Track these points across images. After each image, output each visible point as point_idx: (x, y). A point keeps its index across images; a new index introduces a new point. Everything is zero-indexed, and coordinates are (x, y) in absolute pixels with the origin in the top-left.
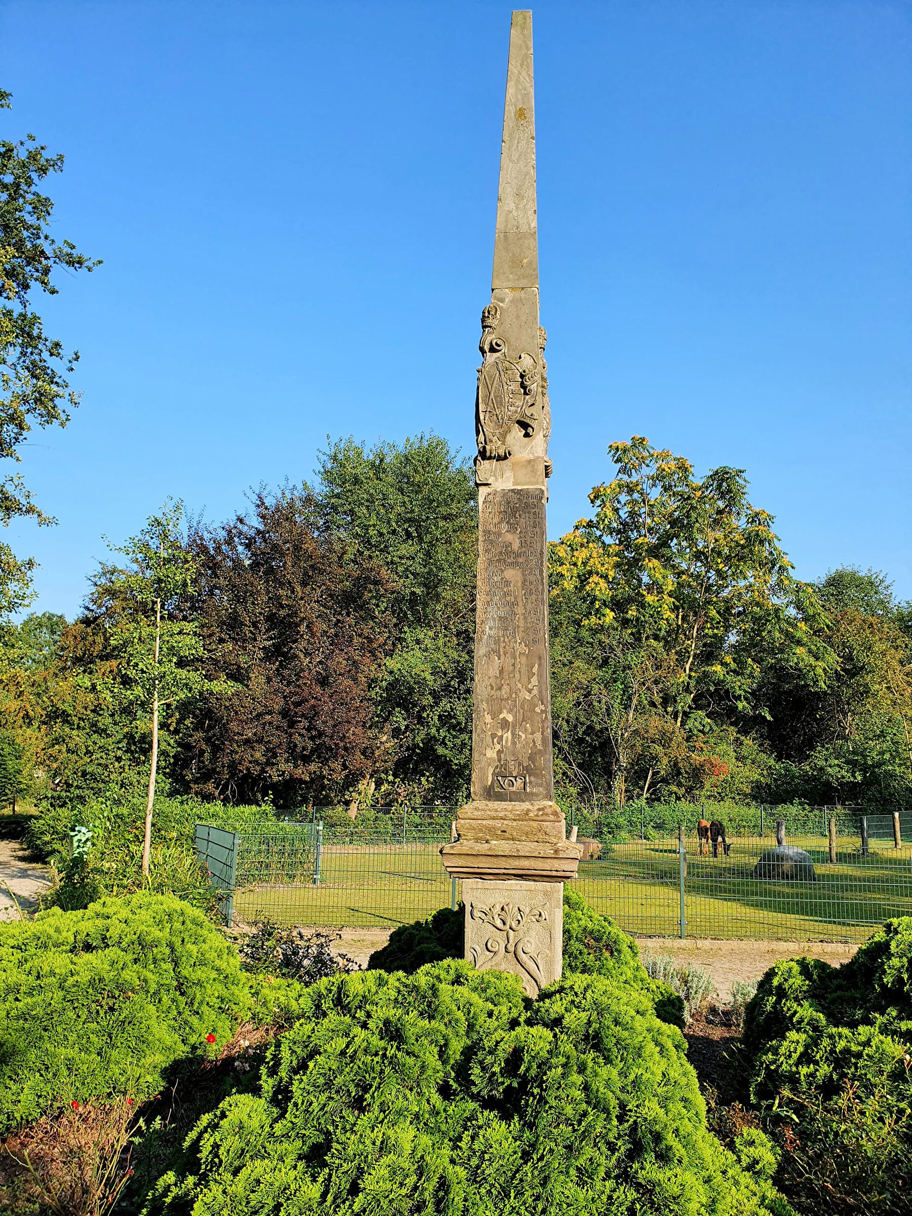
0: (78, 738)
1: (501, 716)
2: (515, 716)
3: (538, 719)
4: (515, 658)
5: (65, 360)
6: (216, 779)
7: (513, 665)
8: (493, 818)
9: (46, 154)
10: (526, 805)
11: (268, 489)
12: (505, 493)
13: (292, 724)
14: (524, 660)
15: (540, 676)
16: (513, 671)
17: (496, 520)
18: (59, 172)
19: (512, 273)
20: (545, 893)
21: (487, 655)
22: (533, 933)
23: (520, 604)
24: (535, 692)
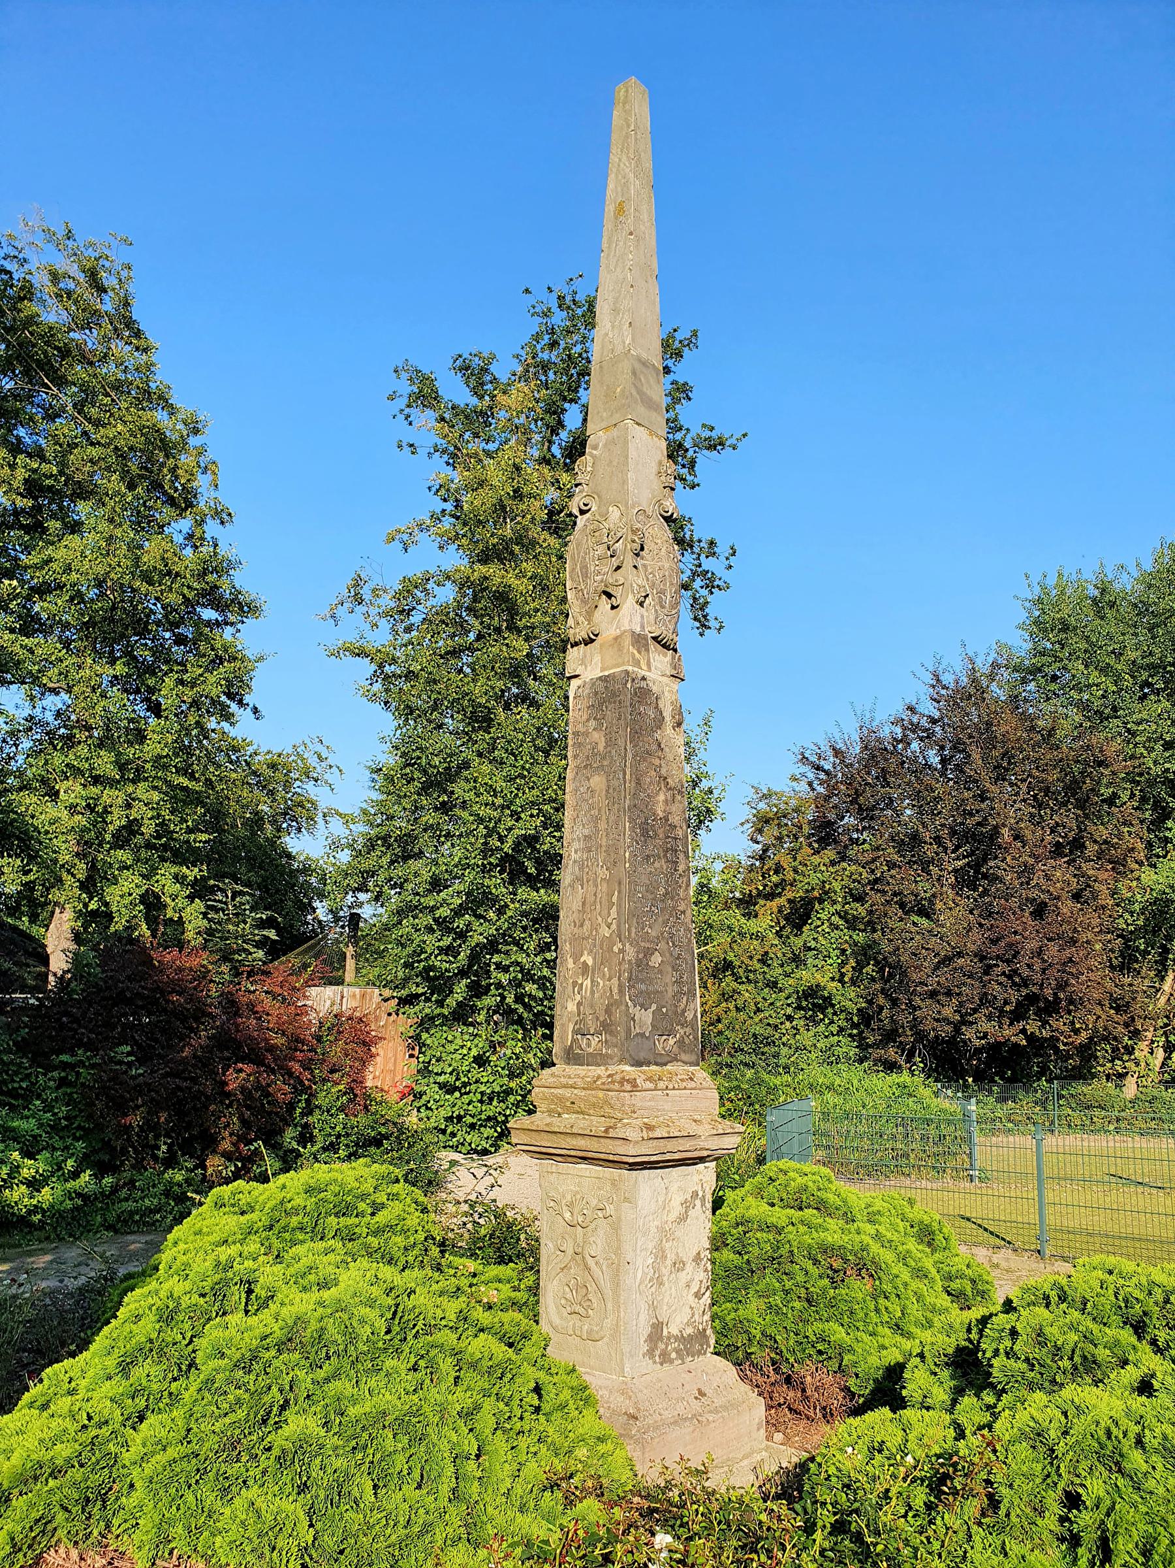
0: (747, 993)
1: (582, 960)
2: (594, 959)
3: (615, 961)
4: (597, 886)
5: (722, 558)
6: (901, 1043)
7: (595, 895)
8: (565, 1086)
9: (679, 336)
10: (600, 1071)
11: (944, 663)
12: (593, 682)
13: (987, 970)
14: (605, 885)
15: (619, 906)
16: (595, 902)
17: (585, 717)
18: (695, 350)
19: (605, 410)
20: (614, 1183)
21: (572, 886)
22: (601, 1232)
23: (604, 817)
24: (614, 926)
